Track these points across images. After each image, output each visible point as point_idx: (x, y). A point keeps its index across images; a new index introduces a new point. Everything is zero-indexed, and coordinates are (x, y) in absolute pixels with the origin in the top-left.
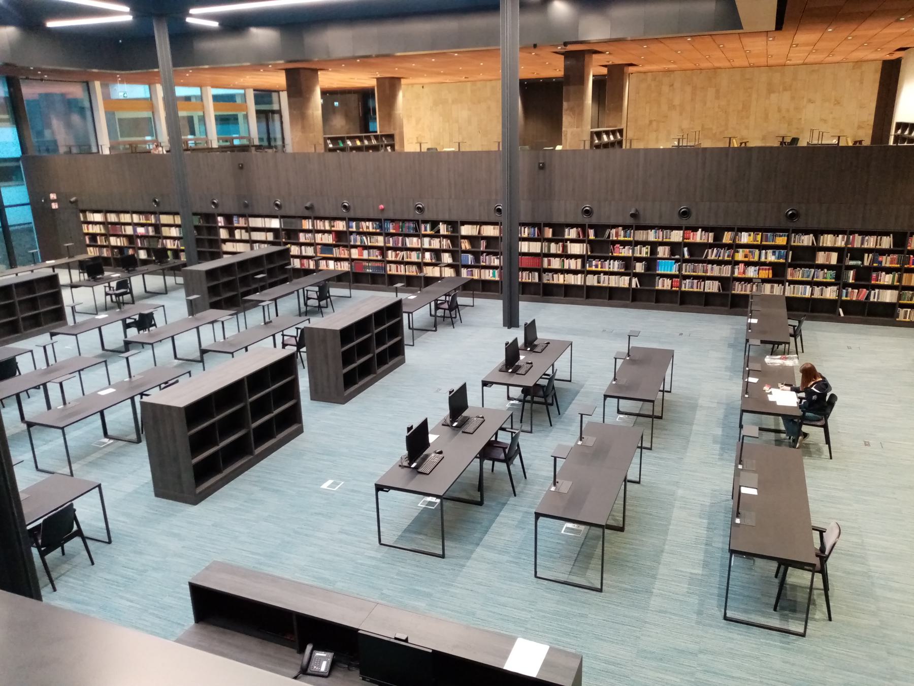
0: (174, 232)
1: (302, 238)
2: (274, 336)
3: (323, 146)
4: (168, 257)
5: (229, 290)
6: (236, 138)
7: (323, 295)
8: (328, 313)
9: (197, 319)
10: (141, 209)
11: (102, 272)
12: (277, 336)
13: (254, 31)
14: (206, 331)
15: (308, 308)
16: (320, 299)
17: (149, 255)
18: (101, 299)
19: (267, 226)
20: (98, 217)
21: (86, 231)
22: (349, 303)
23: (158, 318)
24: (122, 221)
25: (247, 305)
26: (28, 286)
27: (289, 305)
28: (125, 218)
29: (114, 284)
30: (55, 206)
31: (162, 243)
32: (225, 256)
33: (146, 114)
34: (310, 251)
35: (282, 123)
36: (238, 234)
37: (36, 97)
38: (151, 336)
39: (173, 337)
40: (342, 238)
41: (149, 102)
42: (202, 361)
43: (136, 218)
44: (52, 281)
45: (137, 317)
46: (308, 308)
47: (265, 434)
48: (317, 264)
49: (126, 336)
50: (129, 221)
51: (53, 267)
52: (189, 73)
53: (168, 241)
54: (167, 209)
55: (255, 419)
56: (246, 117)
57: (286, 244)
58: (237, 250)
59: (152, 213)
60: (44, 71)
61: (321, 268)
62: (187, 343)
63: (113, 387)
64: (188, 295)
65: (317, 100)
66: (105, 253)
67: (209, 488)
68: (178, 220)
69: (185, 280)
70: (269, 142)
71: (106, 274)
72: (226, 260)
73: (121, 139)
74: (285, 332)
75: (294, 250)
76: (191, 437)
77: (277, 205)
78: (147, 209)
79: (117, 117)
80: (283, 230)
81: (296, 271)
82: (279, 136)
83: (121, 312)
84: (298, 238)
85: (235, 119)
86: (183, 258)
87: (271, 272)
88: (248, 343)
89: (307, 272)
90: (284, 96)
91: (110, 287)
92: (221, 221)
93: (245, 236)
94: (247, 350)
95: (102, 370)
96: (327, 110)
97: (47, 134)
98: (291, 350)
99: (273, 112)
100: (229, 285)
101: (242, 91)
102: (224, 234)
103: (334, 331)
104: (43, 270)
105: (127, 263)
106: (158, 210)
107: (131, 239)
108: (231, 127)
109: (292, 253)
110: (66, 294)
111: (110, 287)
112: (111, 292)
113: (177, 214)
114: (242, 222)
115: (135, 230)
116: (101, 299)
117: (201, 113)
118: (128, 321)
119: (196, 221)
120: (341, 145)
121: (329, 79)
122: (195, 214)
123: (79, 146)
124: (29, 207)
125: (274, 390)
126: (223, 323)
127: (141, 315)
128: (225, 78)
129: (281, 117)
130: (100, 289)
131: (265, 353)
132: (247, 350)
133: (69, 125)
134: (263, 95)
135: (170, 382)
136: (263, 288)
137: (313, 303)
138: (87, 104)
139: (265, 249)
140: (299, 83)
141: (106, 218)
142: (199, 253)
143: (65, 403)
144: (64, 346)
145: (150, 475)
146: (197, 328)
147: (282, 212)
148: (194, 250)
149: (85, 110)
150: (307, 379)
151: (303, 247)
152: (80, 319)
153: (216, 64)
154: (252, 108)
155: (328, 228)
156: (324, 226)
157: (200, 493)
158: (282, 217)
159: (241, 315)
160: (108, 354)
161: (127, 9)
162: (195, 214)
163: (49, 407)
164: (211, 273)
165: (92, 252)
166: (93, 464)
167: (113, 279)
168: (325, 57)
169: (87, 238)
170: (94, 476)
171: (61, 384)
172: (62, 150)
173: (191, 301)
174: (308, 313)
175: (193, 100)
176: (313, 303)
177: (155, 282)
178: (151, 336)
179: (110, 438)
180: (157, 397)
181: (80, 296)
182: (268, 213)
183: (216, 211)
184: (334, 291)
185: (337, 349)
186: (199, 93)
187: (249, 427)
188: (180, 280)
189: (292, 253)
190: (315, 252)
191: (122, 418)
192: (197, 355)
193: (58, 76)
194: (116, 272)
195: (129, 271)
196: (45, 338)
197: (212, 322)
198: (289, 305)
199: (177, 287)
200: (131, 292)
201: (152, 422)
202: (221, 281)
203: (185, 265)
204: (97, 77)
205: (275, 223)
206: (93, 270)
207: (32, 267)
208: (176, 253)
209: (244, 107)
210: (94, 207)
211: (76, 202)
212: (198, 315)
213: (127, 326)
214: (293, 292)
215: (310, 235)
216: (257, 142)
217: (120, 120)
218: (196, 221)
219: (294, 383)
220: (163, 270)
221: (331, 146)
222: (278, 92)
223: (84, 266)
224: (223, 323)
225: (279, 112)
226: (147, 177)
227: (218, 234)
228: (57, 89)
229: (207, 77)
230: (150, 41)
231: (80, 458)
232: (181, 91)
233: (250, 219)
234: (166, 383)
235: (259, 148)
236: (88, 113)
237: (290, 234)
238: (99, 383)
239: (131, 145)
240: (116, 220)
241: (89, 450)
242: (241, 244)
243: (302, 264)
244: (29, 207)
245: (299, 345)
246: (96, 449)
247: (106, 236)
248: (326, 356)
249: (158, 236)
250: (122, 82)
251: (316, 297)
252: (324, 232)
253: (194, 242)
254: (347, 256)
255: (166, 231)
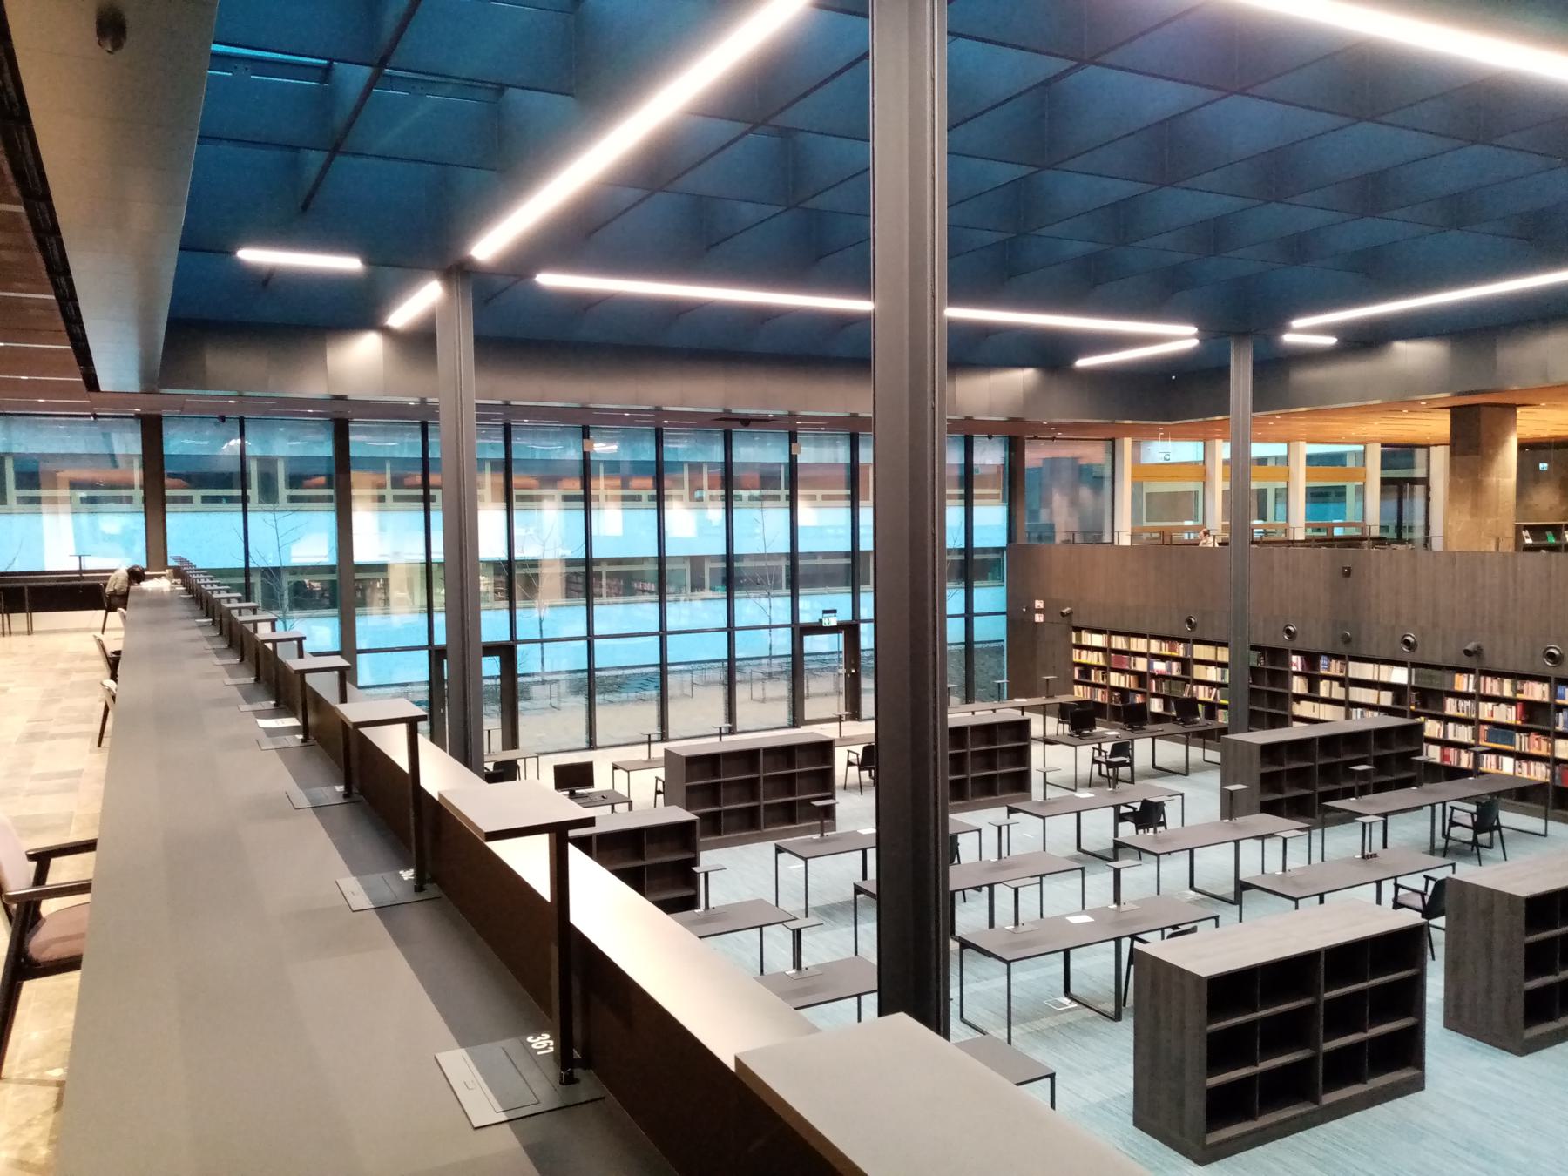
0: (1213, 674)
1: (1451, 707)
2: (1379, 883)
3: (1512, 542)
4: (1197, 714)
5: (1302, 785)
6: (1339, 525)
7: (1485, 821)
8: (1489, 859)
9: (1237, 827)
10: (1166, 633)
11: (1093, 726)
12: (1384, 884)
13: (1400, 346)
14: (1250, 850)
15: (1451, 843)
16: (1478, 828)
17: (1166, 707)
18: (1085, 768)
19: (1383, 679)
20: (1098, 640)
21: (1076, 659)
22: (1540, 848)
23: (1171, 812)
24: (1134, 648)
25: (1329, 816)
26: (988, 731)
27: (1411, 830)
28: (1139, 645)
29: (1107, 747)
30: (1039, 618)
31: (1191, 691)
32: (1296, 724)
33: (1191, 486)
34: (1464, 734)
35: (1428, 499)
36: (1324, 689)
37: (1040, 464)
38: (1158, 841)
39: (1192, 851)
40: (1536, 717)
41: (1200, 471)
42: (1237, 901)
43: (1155, 647)
44: (1020, 729)
45: (1138, 806)
46: (1451, 843)
47: (1345, 1068)
48: (1477, 760)
49: (1116, 835)
50: (1143, 649)
51: (1023, 709)
52: (1275, 420)
53: (1201, 688)
54: (1207, 637)
55: (1331, 1033)
56: (1361, 491)
57: (1415, 715)
58: (1319, 717)
59: (1181, 640)
60: (1059, 426)
61: (1483, 769)
62: (1215, 866)
63: (1090, 913)
64: (1224, 781)
65: (1509, 455)
66: (1100, 696)
67: (1340, 1102)
68: (1223, 655)
69: (1223, 757)
70: (1398, 532)
71: (1098, 729)
72: (1296, 732)
73: (1145, 524)
74: (1400, 881)
75: (1432, 728)
76: (1529, 947)
77: (1407, 643)
78: (1176, 634)
79: (1145, 491)
80: (1414, 689)
81: (1430, 766)
82: (1419, 522)
83: (1114, 793)
84: (1443, 708)
85: (1340, 493)
86: (1222, 718)
87: (1380, 763)
88: (1328, 891)
89: (1455, 773)
90: (1440, 456)
91: (1100, 750)
92: (1296, 662)
93: (1338, 692)
94: (1322, 901)
95: (1074, 881)
96: (1527, 476)
97: (1044, 517)
98: (1414, 918)
99: (1414, 481)
100: (1300, 777)
101: (1360, 448)
102: (1298, 685)
103: (1512, 898)
104: (1007, 712)
105: (1133, 716)
106: (1191, 636)
107: (1141, 677)
108: (1332, 507)
109: (1427, 734)
110: (1036, 750)
111: (1100, 750)
112: (1102, 759)
113: (1224, 645)
114: (1335, 668)
115: (1150, 665)
116: (1085, 768)
117: (1282, 485)
118: (1124, 810)
119: (1254, 659)
120: (1551, 540)
121: (1536, 422)
122: (1253, 648)
123: (1084, 534)
124: (1004, 617)
125: (1374, 989)
126: (1285, 840)
127: (1145, 803)
128: (1336, 426)
129: (1428, 489)
130: (1086, 752)
131: (1360, 914)
132: (1322, 901)
133: (1074, 502)
134: (1398, 454)
135: (1183, 928)
136: (1363, 791)
137: (1463, 834)
138: (1108, 472)
139: (1375, 721)
140: (1473, 433)
141: (1109, 642)
142: (1252, 712)
143: (1016, 923)
144: (1025, 831)
145: (1130, 1084)
146: (1237, 842)
147: (1416, 657)
148: (1244, 706)
149: (1098, 480)
150: (1442, 984)
151: (1451, 725)
152: (1053, 793)
153: (1322, 404)
154: (1374, 473)
155: (1508, 693)
156: (1501, 689)
157: (1212, 1145)
158: (1415, 665)
159: (1317, 833)
160: (1084, 858)
161: (1193, 330)
162: (1253, 648)
163: (991, 925)
164: (1269, 750)
165: (1080, 693)
166: (1040, 1035)
167: (1105, 738)
168: (1537, 382)
169: (1076, 670)
170: (1045, 1057)
171: (1016, 890)
172: (1060, 538)
173: (1231, 792)
174: (1450, 850)
175: (1271, 463)
176: (1463, 834)
177: (1171, 752)
178: (1158, 841)
179: (1073, 999)
180: (1155, 946)
181: (1056, 760)
182: (1387, 656)
183: (1290, 646)
184: (1507, 818)
185: (1515, 938)
186: (1287, 454)
187: (1316, 1047)
188: (1214, 756)
189: (1427, 734)
190: (1476, 736)
191: (1096, 968)
192: (1229, 889)
193: (1077, 432)
194: (1112, 728)
195: (1133, 730)
196: (998, 814)
197: (1262, 837)
198: (1411, 830)
199: (1207, 765)
200: (1131, 764)
201: (1150, 990)
202: (1287, 767)
203: (1224, 731)
204: (1128, 431)
205: (1399, 676)
206: (1080, 719)
207: (995, 705)
208: (1211, 709)
209: (1360, 473)
210: (1095, 626)
211: (1069, 614)
212: (1240, 820)
213: (1120, 818)
214: (1420, 808)
215: (1468, 703)
216: (1376, 532)
217: (1149, 495)
218: (1254, 659)
219: (1415, 987)
220: (1187, 734)
221: (1529, 541)
222: (1427, 447)
223: (1064, 712)
224: (1285, 840)
225: (1426, 482)
226: (1187, 582)
227: (1288, 685)
228: (1065, 451)
229: (1301, 425)
230: (1223, 372)
231: (1025, 1020)
232: (1258, 450)
233: (1351, 664)
234: (1175, 927)
235: (1380, 541)
236: (1107, 484)
237: (1429, 699)
238: (1070, 902)
239: (1162, 533)
240: (1125, 647)
241: (1041, 1010)
242: (1329, 707)
243: (1444, 757)
244: (1004, 617)
245: (1429, 911)
246: (1050, 1012)
247: (1105, 670)
248: (1489, 946)
249: (1186, 678)
250: (1165, 438)
251: (1469, 822)
252: (1498, 700)
253: (1247, 696)
254: (1544, 752)
255: (1199, 672)
